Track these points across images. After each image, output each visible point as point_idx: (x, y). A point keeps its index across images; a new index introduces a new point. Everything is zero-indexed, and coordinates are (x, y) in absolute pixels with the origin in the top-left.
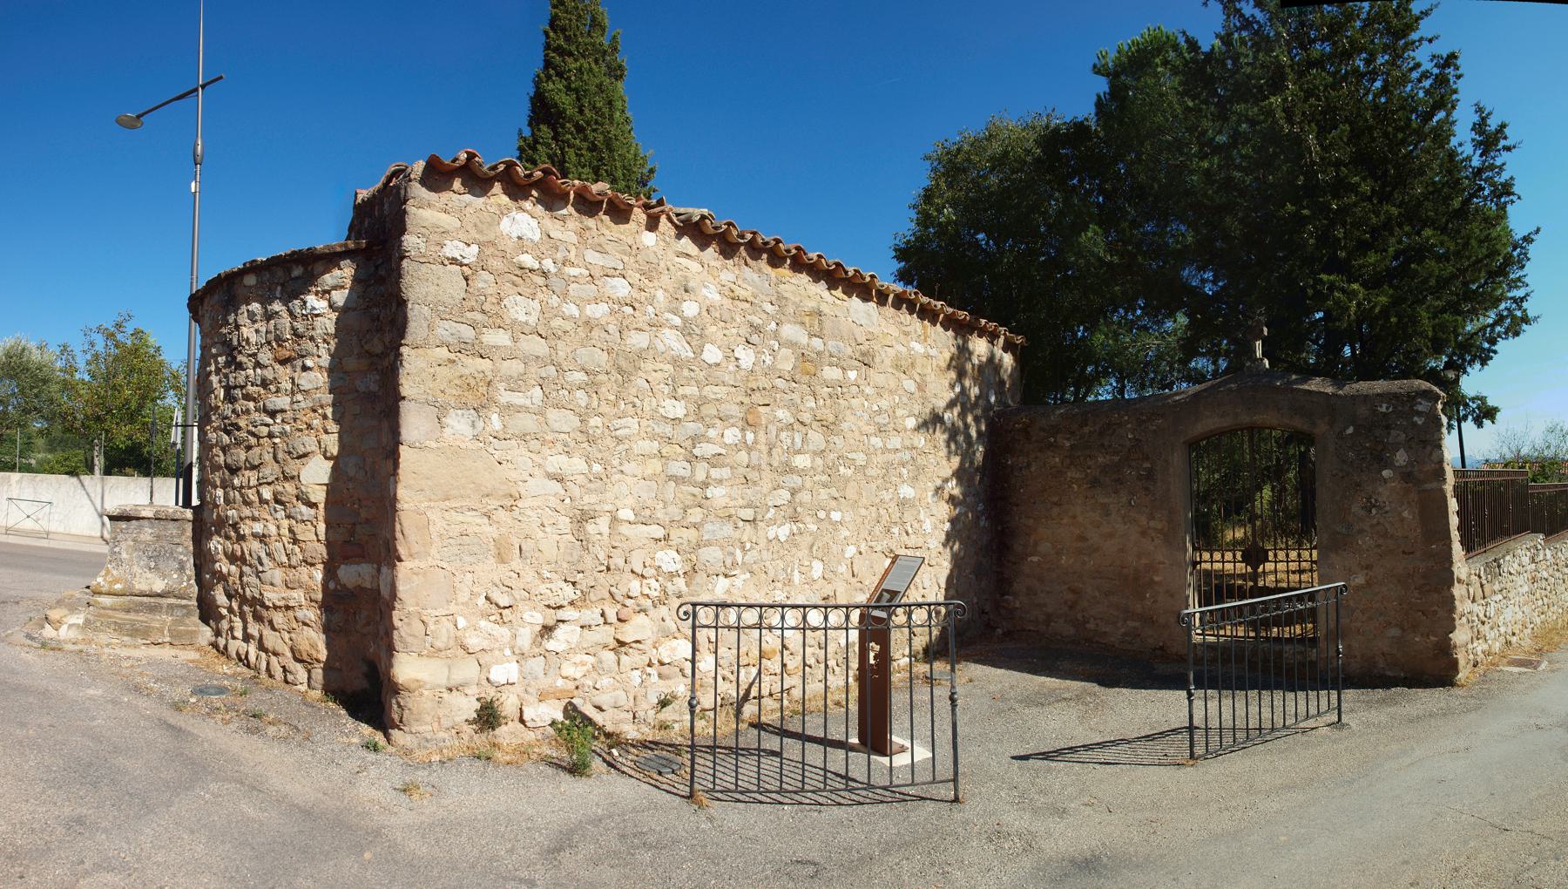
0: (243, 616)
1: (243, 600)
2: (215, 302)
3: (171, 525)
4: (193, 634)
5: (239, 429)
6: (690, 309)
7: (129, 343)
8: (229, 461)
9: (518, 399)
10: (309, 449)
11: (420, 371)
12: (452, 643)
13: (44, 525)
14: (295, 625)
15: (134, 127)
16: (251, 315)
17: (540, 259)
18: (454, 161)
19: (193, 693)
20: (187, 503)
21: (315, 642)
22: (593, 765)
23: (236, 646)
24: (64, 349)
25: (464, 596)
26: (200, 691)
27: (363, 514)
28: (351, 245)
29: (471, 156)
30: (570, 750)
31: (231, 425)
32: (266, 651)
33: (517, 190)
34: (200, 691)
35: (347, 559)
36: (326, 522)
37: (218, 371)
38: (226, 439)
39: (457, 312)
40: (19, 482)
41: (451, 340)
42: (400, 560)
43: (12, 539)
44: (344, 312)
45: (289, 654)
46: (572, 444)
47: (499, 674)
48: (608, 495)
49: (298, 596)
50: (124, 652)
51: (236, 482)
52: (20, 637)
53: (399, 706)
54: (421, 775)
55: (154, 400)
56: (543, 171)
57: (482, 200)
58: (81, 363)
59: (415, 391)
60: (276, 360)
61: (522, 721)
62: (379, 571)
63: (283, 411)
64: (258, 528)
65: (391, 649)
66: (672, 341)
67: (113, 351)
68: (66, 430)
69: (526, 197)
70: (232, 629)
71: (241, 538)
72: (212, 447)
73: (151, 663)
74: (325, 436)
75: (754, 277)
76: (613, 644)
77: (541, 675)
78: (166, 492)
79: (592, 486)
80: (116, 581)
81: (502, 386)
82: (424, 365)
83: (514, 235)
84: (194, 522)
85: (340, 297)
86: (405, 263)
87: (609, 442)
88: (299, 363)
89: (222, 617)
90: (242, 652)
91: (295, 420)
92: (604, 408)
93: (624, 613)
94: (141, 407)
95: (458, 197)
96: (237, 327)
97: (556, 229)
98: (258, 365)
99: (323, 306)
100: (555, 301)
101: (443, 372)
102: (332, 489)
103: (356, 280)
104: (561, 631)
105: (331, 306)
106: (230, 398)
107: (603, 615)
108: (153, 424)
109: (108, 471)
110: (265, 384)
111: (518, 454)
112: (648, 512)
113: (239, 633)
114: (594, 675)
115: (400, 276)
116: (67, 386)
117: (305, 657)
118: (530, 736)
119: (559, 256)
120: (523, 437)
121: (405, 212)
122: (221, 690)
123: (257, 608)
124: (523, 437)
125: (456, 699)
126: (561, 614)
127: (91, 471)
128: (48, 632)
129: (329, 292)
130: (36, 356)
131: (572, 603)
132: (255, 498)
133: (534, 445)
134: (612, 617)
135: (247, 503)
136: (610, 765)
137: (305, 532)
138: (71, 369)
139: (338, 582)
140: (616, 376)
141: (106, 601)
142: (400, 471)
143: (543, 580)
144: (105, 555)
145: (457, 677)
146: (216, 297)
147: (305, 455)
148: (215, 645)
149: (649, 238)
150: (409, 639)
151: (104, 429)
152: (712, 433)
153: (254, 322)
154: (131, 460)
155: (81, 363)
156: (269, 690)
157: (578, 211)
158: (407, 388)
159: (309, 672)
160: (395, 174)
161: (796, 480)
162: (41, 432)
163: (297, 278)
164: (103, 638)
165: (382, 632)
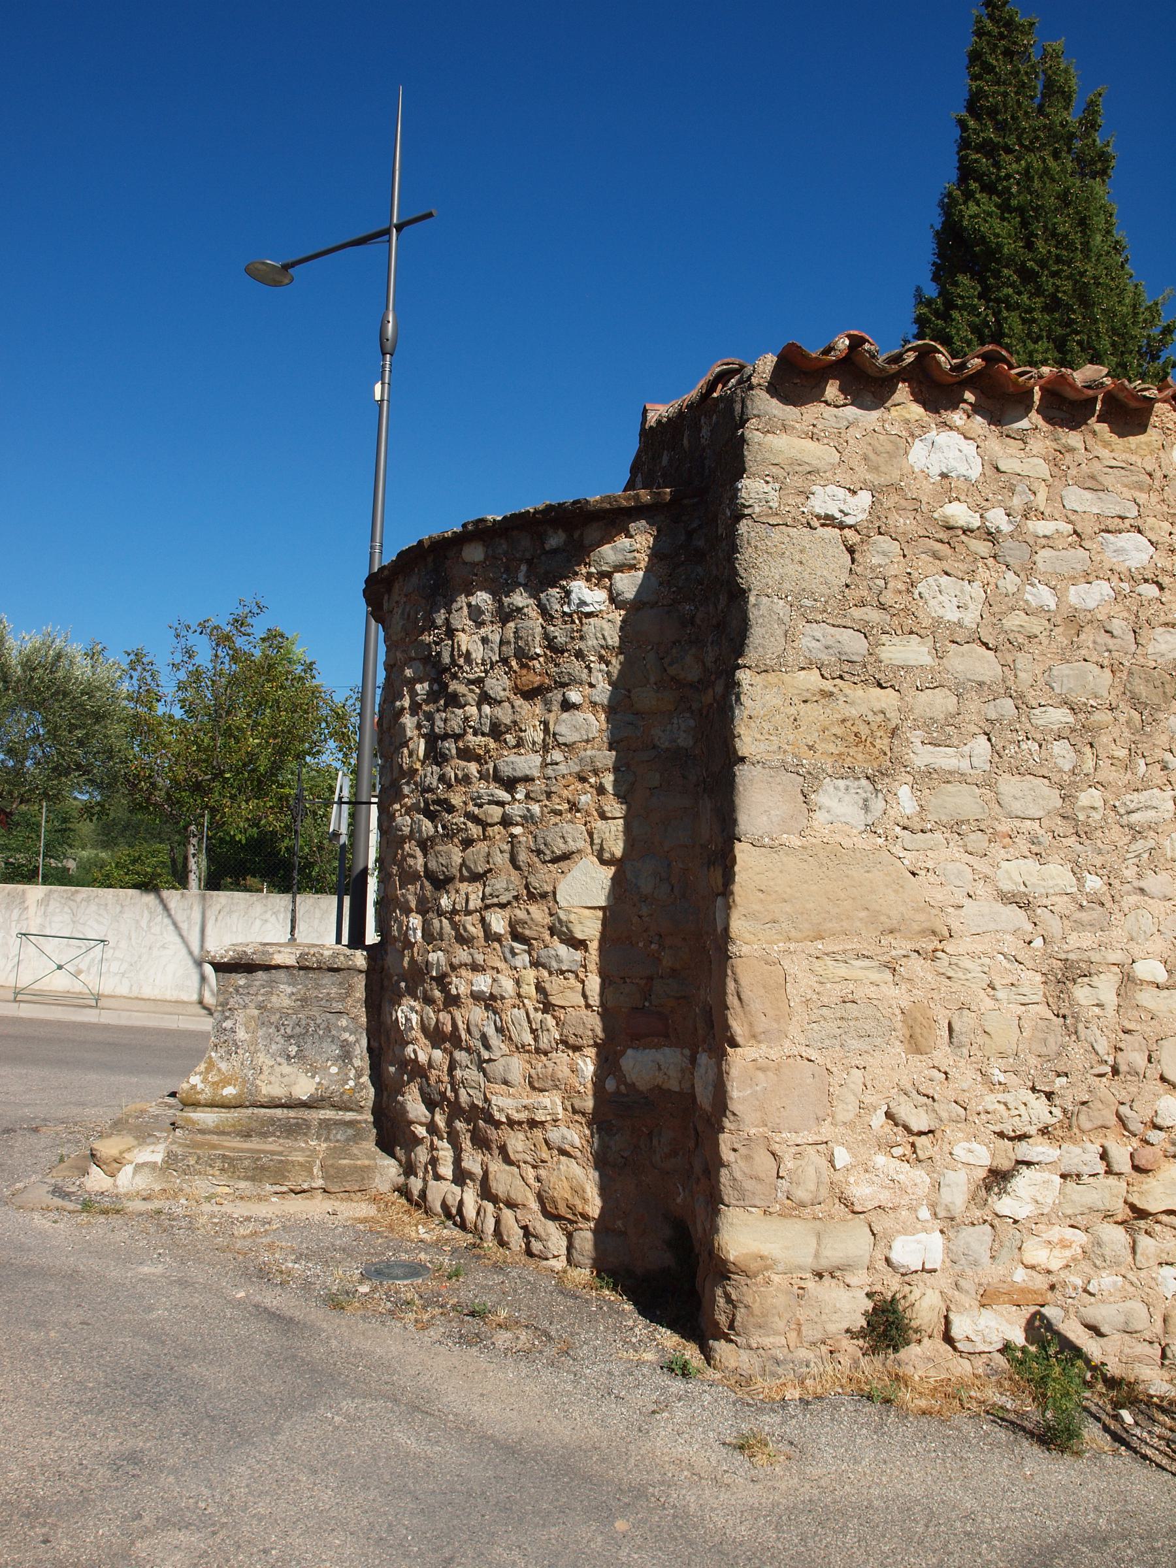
0: (454, 1139)
1: (455, 1111)
2: (410, 589)
3: (327, 979)
4: (364, 1172)
5: (451, 809)
7: (258, 653)
8: (433, 865)
9: (945, 759)
10: (572, 846)
11: (771, 710)
12: (824, 1192)
13: (91, 982)
14: (545, 1155)
15: (277, 284)
16: (475, 613)
17: (982, 511)
18: (827, 351)
19: (364, 1277)
20: (357, 939)
21: (580, 1183)
22: (1085, 1432)
23: (442, 1191)
24: (137, 659)
25: (846, 1111)
26: (377, 1272)
27: (667, 961)
28: (645, 496)
29: (856, 342)
30: (1041, 1400)
31: (438, 802)
32: (494, 1199)
33: (937, 395)
34: (377, 1272)
35: (637, 1039)
36: (602, 973)
37: (415, 708)
38: (427, 827)
39: (836, 609)
40: (44, 902)
41: (825, 657)
42: (734, 1044)
43: (26, 1011)
44: (635, 612)
45: (535, 1206)
46: (1047, 839)
47: (906, 1252)
48: (1116, 933)
49: (551, 1103)
50: (239, 1210)
51: (445, 902)
52: (42, 1194)
53: (729, 1300)
54: (769, 1421)
55: (300, 756)
56: (984, 357)
57: (875, 414)
58: (168, 685)
59: (762, 747)
60: (517, 690)
61: (948, 1339)
62: (693, 1060)
63: (528, 779)
64: (482, 983)
65: (714, 1201)
67: (228, 667)
68: (137, 807)
70: (434, 1161)
71: (453, 1001)
72: (403, 840)
73: (289, 1226)
74: (600, 824)
76: (1123, 1212)
77: (985, 1259)
78: (318, 922)
79: (1083, 916)
80: (226, 1082)
81: (916, 737)
82: (778, 702)
83: (935, 471)
84: (369, 973)
85: (628, 584)
86: (743, 527)
87: (1116, 835)
88: (556, 696)
89: (418, 1141)
90: (453, 1203)
91: (549, 795)
92: (1107, 773)
93: (1146, 1156)
94: (276, 767)
95: (833, 411)
96: (451, 633)
97: (1010, 457)
98: (485, 698)
99: (599, 599)
100: (1010, 582)
101: (813, 713)
102: (612, 916)
103: (656, 554)
104: (1023, 1182)
105: (612, 600)
106: (435, 756)
107: (1104, 1156)
108: (299, 798)
109: (213, 883)
110: (496, 731)
111: (948, 857)
113: (447, 1170)
114: (1086, 1266)
115: (734, 549)
116: (140, 727)
117: (563, 1211)
118: (964, 1368)
119: (1017, 502)
120: (956, 827)
121: (743, 440)
122: (414, 1270)
123: (478, 1124)
124: (956, 827)
125: (827, 1292)
126: (1024, 1150)
127: (180, 880)
128: (97, 1180)
129: (609, 575)
130: (82, 669)
131: (1044, 1131)
132: (476, 931)
133: (976, 840)
134: (1122, 1162)
135: (464, 940)
136: (1116, 1438)
137: (565, 993)
138: (148, 696)
139: (621, 1079)
140: (1127, 713)
141: (207, 1117)
142: (736, 888)
143: (991, 1085)
144: (205, 1035)
145: (833, 1254)
146: (414, 580)
147: (566, 857)
148: (403, 1191)
150: (749, 1185)
151: (203, 806)
153: (480, 624)
154: (257, 864)
155: (168, 685)
156: (498, 1268)
157: (1049, 420)
158: (748, 741)
159: (570, 1236)
160: (723, 377)
162: (87, 810)
163: (555, 551)
164: (200, 1186)
165: (698, 1168)
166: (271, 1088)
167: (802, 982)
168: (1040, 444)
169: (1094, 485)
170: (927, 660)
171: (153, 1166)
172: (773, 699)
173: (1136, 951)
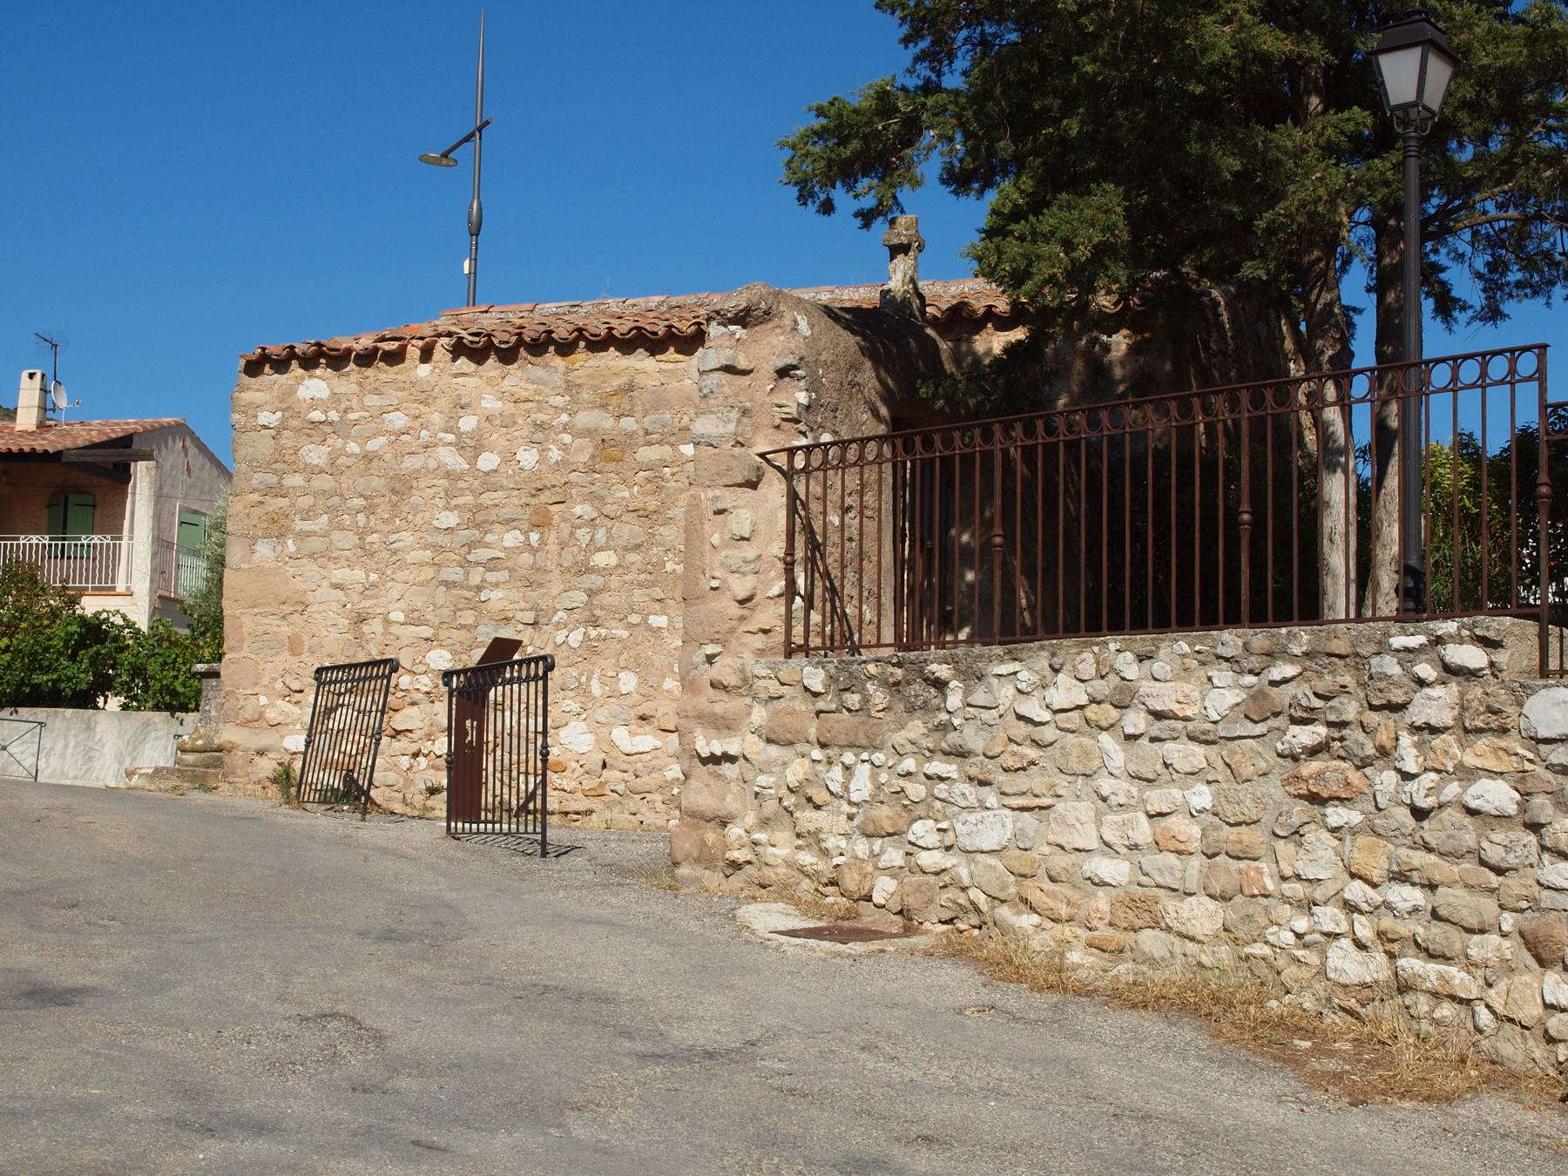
6: (468, 423)
9: (307, 526)
25: (265, 681)
29: (263, 349)
39: (267, 467)
66: (452, 459)
69: (317, 366)
75: (522, 376)
87: (385, 555)
101: (258, 511)
111: (310, 569)
112: (416, 614)
120: (311, 556)
149: (424, 370)
152: (489, 538)
157: (358, 365)
161: (597, 581)
167: (248, 624)
168: (354, 377)
170: (302, 483)
172: (239, 507)
173: (391, 607)
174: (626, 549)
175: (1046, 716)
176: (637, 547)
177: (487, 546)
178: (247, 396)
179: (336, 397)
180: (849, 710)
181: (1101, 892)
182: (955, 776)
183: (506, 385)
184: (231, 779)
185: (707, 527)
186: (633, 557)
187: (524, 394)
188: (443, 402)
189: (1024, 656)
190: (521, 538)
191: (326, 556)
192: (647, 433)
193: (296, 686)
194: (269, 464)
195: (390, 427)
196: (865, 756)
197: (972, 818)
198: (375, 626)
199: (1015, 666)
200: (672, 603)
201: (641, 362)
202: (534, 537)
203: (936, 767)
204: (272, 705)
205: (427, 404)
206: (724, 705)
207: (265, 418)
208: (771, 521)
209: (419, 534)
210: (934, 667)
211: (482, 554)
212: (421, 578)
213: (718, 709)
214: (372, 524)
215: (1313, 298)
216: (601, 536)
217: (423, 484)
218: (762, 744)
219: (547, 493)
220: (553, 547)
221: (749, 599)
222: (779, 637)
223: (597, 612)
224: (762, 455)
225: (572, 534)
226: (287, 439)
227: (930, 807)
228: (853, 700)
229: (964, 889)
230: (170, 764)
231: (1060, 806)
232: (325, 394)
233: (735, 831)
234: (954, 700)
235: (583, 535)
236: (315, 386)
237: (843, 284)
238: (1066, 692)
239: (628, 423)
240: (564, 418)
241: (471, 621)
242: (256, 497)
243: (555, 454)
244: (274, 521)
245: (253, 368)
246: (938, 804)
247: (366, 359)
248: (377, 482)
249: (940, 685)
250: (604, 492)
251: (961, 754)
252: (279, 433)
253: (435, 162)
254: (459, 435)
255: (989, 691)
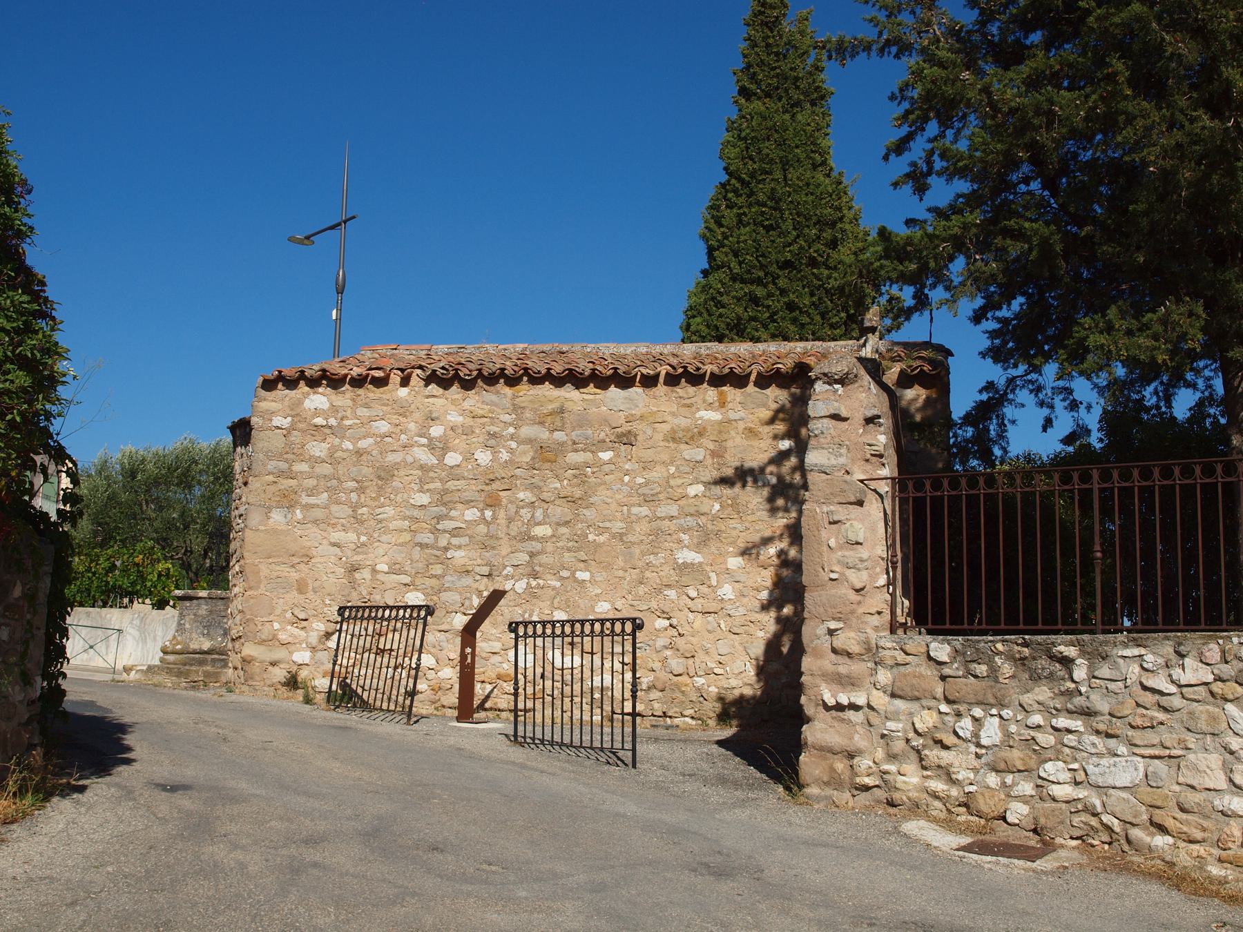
6: (436, 431)
9: (312, 500)
25: (278, 612)
29: (280, 372)
39: (280, 456)
66: (424, 456)
69: (319, 385)
75: (476, 400)
87: (373, 523)
101: (273, 488)
111: (313, 531)
149: (403, 392)
152: (453, 513)
161: (537, 546)
166: (194, 646)
167: (264, 570)
169: (367, 406)
171: (142, 671)
172: (258, 485)
173: (377, 561)
174: (558, 524)
175: (1173, 689)
176: (567, 523)
177: (452, 519)
178: (264, 405)
179: (334, 409)
180: (976, 677)
181: (1232, 822)
182: (1082, 729)
183: (466, 405)
184: (250, 683)
185: (824, 533)
186: (563, 530)
187: (481, 412)
188: (417, 415)
189: (1148, 643)
190: (478, 514)
191: (326, 523)
192: (574, 443)
193: (302, 616)
194: (281, 454)
195: (376, 431)
196: (994, 711)
197: (1104, 761)
198: (366, 574)
199: (1143, 651)
200: (593, 563)
201: (569, 393)
202: (488, 514)
203: (1062, 722)
204: (283, 629)
205: (405, 416)
206: (845, 666)
207: (278, 421)
208: (873, 530)
209: (399, 509)
210: (1062, 648)
211: (448, 525)
212: (401, 541)
213: (843, 670)
214: (362, 500)
215: (1236, 383)
216: (539, 514)
217: (402, 473)
218: (887, 699)
219: (498, 483)
220: (502, 521)
221: (862, 589)
222: (887, 617)
223: (537, 568)
224: (862, 481)
225: (517, 512)
226: (296, 437)
227: (1059, 752)
228: (982, 669)
229: (1095, 815)
230: (157, 662)
231: (1191, 757)
232: (326, 406)
233: (864, 763)
234: (1080, 673)
235: (525, 513)
236: (318, 400)
237: (655, 341)
238: (1192, 672)
239: (560, 436)
240: (511, 430)
241: (439, 572)
242: (271, 478)
243: (504, 456)
244: (285, 496)
245: (269, 385)
246: (1067, 750)
247: (358, 382)
248: (366, 471)
249: (1067, 662)
250: (541, 484)
251: (1087, 713)
252: (289, 433)
253: (300, 242)
254: (430, 439)
255: (1115, 666)
